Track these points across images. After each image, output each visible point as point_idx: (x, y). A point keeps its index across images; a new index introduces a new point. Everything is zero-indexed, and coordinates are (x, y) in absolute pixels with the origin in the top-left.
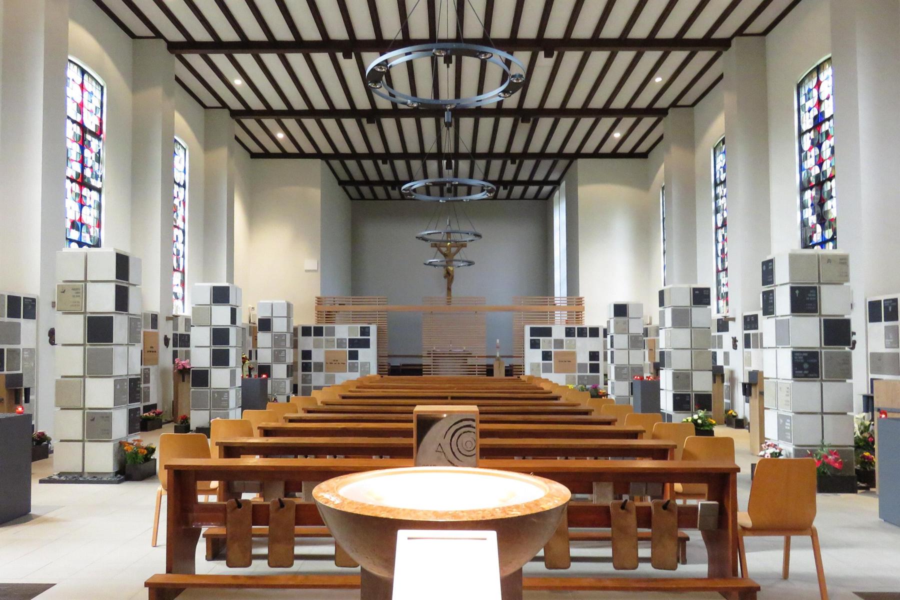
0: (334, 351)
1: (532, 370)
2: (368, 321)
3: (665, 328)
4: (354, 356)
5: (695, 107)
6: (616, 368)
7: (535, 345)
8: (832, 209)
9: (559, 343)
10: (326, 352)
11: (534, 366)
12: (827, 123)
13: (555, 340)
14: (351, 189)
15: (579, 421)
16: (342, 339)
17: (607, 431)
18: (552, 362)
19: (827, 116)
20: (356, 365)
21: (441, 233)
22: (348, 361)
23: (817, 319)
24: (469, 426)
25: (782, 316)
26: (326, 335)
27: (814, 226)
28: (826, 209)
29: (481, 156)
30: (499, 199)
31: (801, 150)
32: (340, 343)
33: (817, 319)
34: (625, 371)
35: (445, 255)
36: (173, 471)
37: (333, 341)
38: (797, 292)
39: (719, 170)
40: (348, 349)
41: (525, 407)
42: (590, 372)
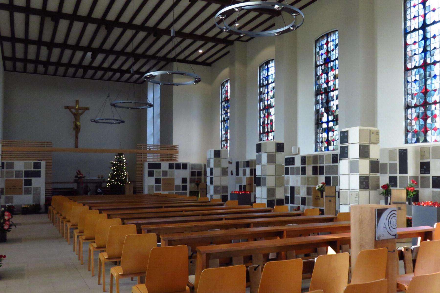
0: (167, 178)
1: (149, 190)
2: (38, 159)
3: (261, 164)
4: (28, 183)
5: (248, 42)
6: (214, 187)
7: (151, 174)
8: (333, 106)
9: (165, 173)
10: (6, 180)
11: (150, 187)
12: (332, 63)
13: (163, 171)
14: (9, 64)
15: (287, 215)
16: (19, 171)
17: (301, 219)
18: (161, 184)
19: (332, 59)
20: (30, 189)
21: (132, 102)
22: (24, 187)
23: (368, 160)
24: (394, 214)
25: (352, 159)
26: (7, 168)
27: (322, 114)
28: (329, 105)
29: (58, 45)
30: (67, 77)
31: (316, 74)
32: (18, 174)
33: (368, 160)
34: (219, 189)
35: (75, 115)
36: (206, 254)
37: (12, 172)
38: (362, 147)
39: (263, 79)
40: (24, 178)
41: (209, 211)
42: (182, 190)
